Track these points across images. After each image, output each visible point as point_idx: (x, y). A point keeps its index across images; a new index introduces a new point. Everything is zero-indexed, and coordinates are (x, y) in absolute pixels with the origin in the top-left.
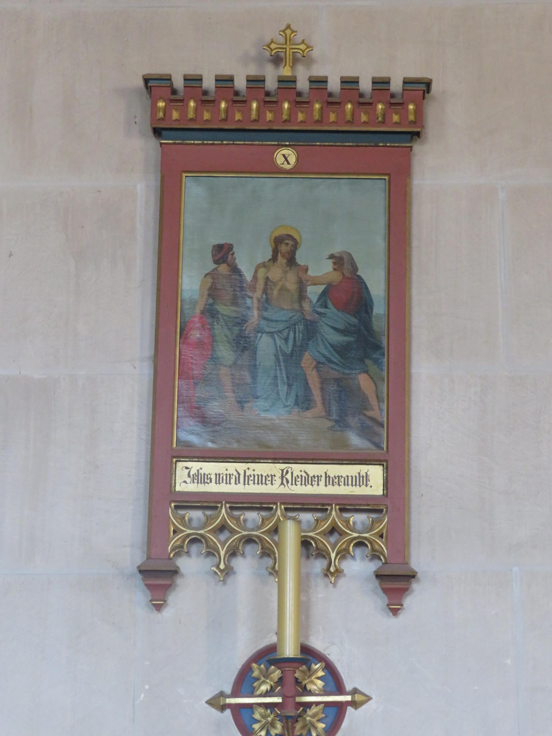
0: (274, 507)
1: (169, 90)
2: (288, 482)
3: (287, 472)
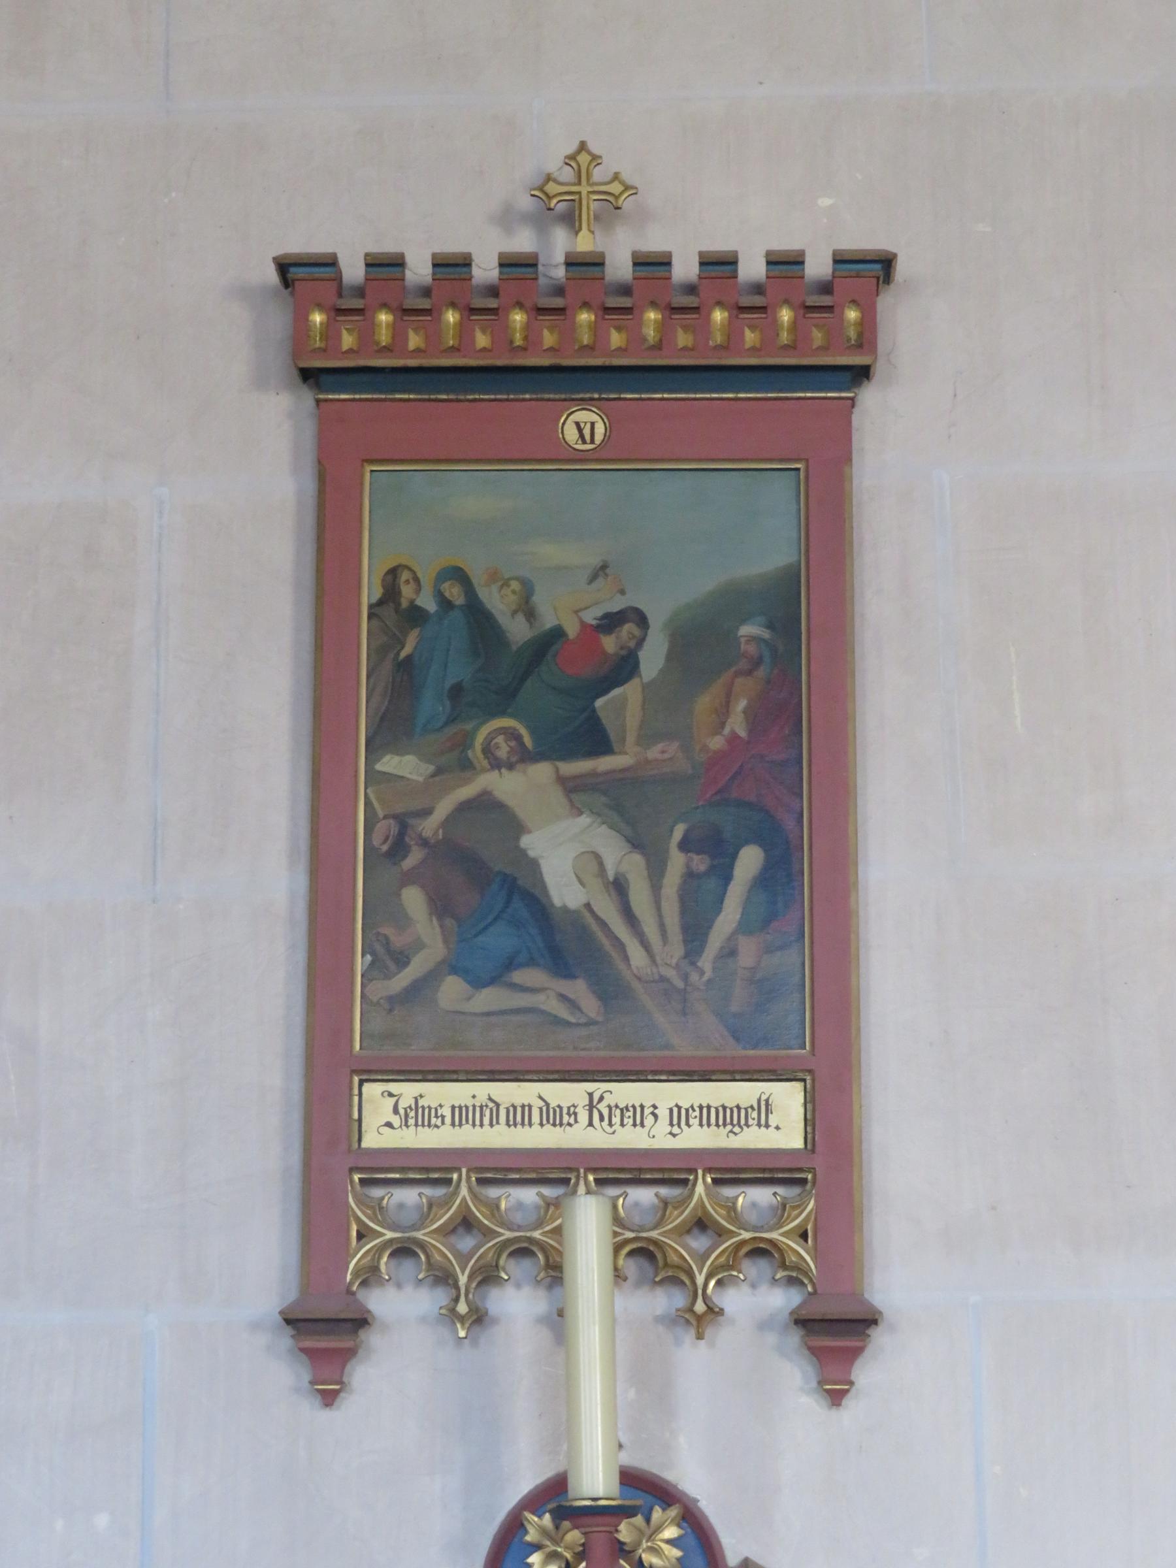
0: (455, 1176)
1: (333, 285)
2: (602, 1118)
3: (601, 1099)
